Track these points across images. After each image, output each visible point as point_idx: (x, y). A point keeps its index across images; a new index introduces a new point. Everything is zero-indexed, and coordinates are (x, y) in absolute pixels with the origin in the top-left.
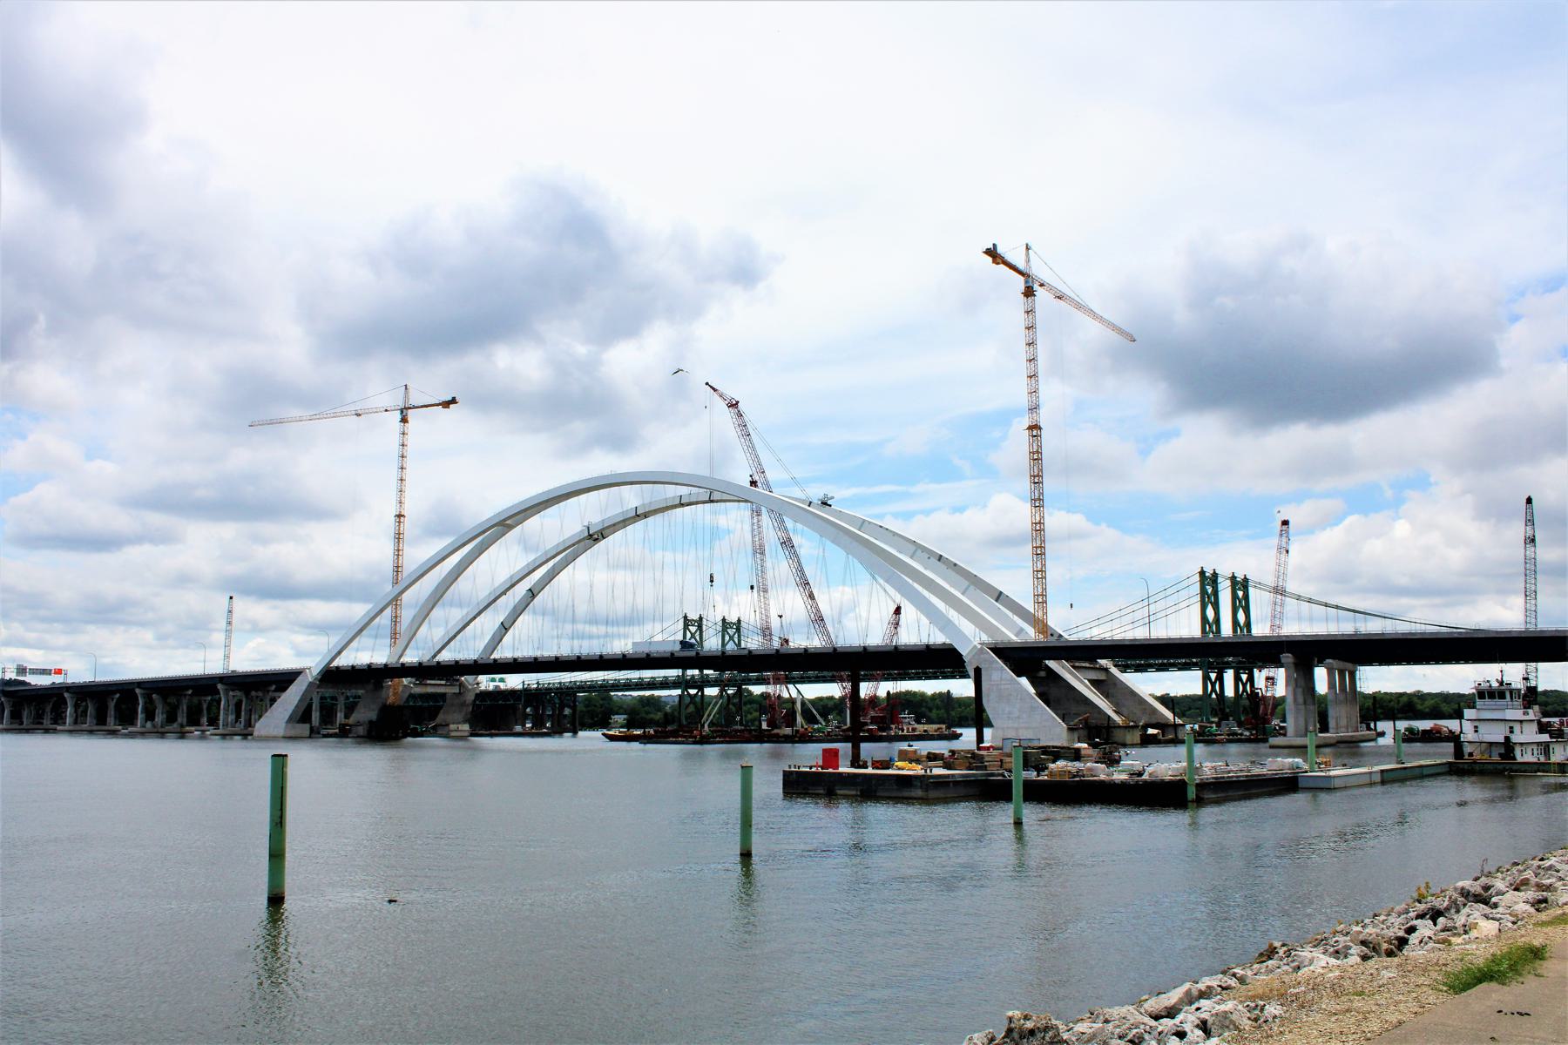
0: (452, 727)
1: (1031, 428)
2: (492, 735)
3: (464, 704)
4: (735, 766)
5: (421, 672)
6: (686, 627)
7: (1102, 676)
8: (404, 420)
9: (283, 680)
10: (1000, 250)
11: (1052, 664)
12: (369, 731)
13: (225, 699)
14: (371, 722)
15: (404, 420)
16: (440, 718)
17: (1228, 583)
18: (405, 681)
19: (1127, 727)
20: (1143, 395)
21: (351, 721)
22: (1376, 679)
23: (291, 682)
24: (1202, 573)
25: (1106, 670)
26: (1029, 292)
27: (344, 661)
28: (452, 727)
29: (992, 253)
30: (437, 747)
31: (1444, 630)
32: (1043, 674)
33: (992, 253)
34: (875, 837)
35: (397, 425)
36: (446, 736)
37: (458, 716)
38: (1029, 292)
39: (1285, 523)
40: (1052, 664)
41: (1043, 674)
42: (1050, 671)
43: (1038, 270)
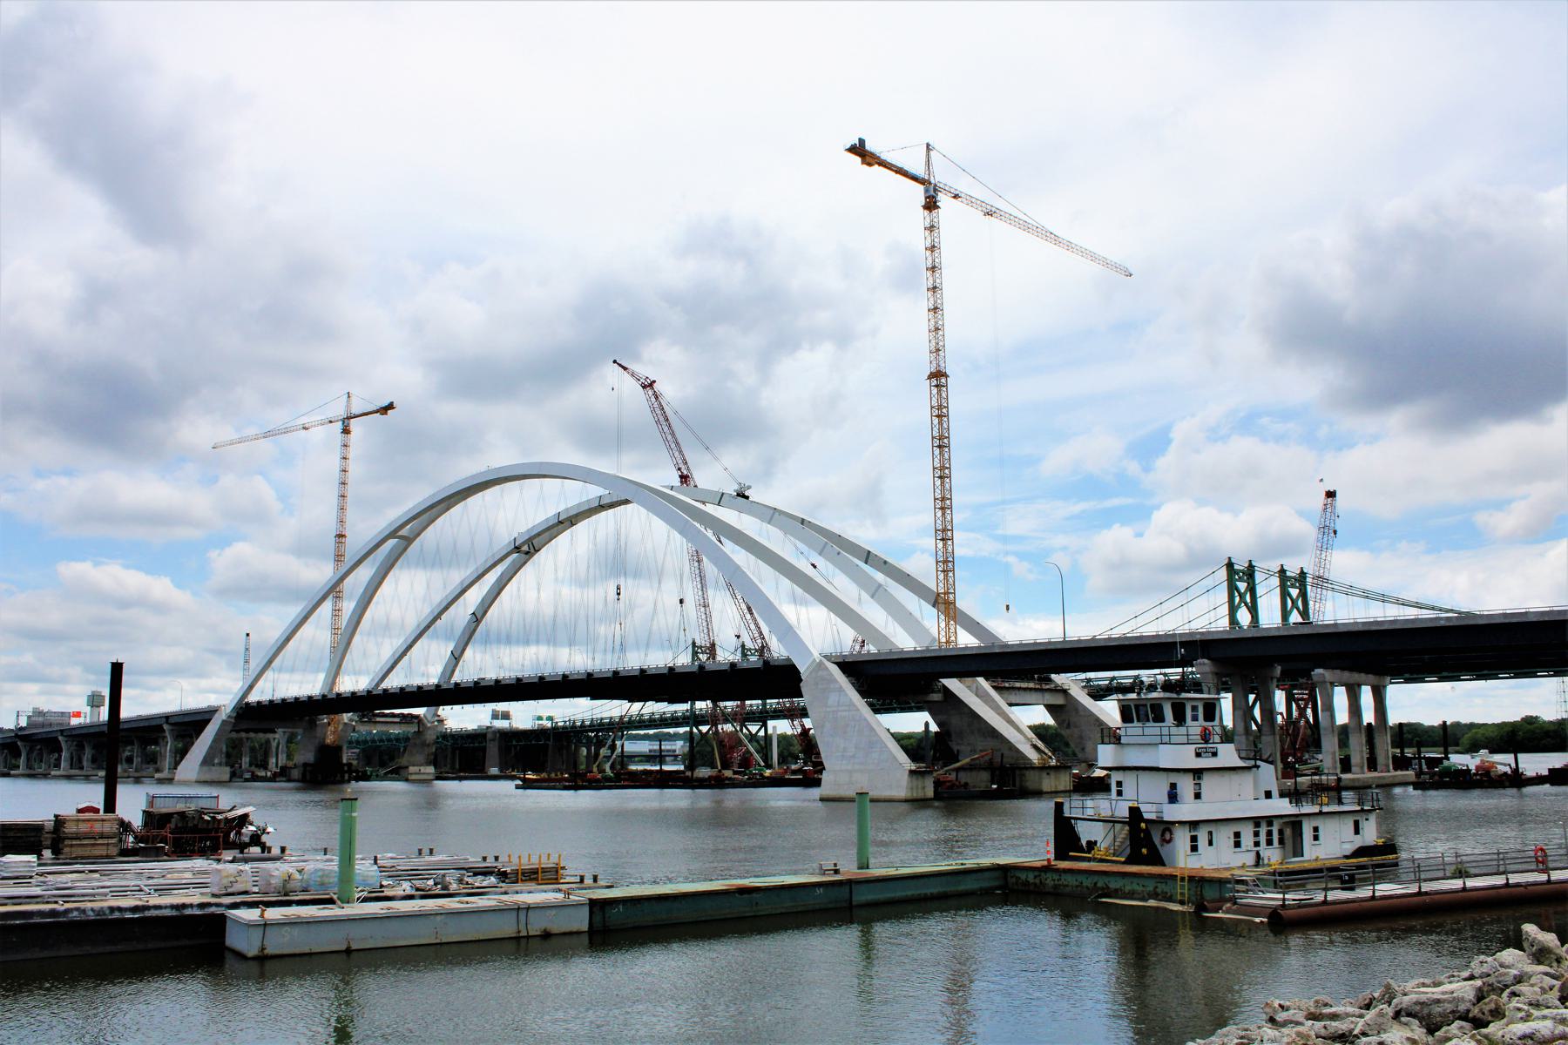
0: (412, 769)
1: (932, 376)
2: (461, 779)
3: (425, 745)
4: (336, 814)
5: (368, 703)
6: (695, 654)
7: (1059, 700)
8: (346, 431)
9: (212, 711)
10: (869, 147)
11: (952, 684)
12: (304, 775)
13: (493, 750)
14: (305, 765)
15: (346, 431)
16: (403, 761)
17: (1276, 581)
18: (346, 717)
19: (1045, 768)
20: (1307, 383)
21: (290, 764)
22: (1419, 703)
23: (207, 722)
24: (1230, 565)
25: (1065, 692)
26: (931, 205)
27: (262, 693)
28: (412, 769)
29: (859, 150)
30: (395, 793)
31: (1410, 613)
32: (936, 697)
33: (859, 150)
34: (256, 935)
35: (339, 437)
36: (407, 780)
37: (420, 758)
38: (931, 205)
39: (1331, 494)
40: (952, 684)
41: (936, 697)
42: (947, 692)
43: (939, 176)
